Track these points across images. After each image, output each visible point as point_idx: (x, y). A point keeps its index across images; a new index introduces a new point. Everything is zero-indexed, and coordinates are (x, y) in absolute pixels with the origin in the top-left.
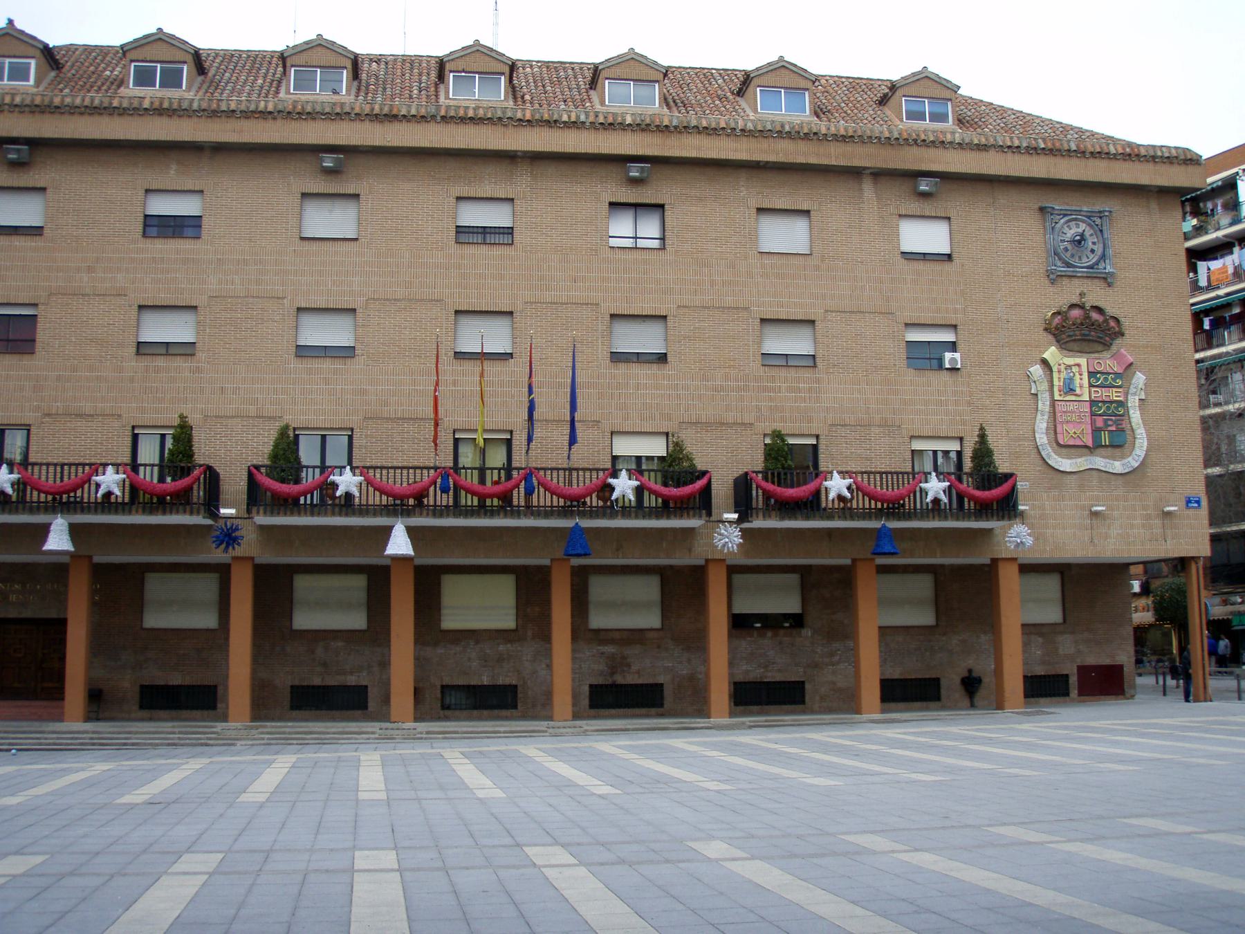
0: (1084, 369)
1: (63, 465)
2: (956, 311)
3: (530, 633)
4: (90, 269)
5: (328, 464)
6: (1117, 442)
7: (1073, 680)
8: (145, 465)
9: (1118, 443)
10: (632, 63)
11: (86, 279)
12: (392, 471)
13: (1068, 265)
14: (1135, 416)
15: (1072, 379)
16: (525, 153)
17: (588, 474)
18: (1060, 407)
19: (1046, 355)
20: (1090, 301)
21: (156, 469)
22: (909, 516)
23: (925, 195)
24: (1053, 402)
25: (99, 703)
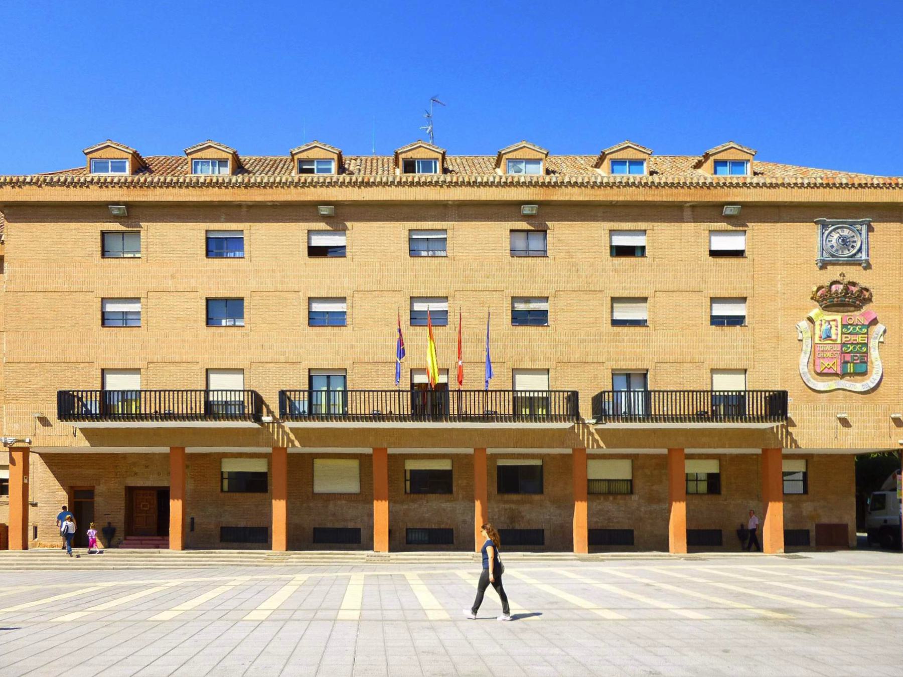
1: (160, 391)
2: (746, 288)
3: (460, 496)
4: (173, 277)
5: (517, 389)
6: (861, 369)
7: (813, 534)
8: (213, 391)
11: (170, 283)
13: (833, 256)
14: (874, 354)
17: (237, 393)
20: (849, 278)
21: (306, 394)
24: (814, 346)
25: (194, 540)
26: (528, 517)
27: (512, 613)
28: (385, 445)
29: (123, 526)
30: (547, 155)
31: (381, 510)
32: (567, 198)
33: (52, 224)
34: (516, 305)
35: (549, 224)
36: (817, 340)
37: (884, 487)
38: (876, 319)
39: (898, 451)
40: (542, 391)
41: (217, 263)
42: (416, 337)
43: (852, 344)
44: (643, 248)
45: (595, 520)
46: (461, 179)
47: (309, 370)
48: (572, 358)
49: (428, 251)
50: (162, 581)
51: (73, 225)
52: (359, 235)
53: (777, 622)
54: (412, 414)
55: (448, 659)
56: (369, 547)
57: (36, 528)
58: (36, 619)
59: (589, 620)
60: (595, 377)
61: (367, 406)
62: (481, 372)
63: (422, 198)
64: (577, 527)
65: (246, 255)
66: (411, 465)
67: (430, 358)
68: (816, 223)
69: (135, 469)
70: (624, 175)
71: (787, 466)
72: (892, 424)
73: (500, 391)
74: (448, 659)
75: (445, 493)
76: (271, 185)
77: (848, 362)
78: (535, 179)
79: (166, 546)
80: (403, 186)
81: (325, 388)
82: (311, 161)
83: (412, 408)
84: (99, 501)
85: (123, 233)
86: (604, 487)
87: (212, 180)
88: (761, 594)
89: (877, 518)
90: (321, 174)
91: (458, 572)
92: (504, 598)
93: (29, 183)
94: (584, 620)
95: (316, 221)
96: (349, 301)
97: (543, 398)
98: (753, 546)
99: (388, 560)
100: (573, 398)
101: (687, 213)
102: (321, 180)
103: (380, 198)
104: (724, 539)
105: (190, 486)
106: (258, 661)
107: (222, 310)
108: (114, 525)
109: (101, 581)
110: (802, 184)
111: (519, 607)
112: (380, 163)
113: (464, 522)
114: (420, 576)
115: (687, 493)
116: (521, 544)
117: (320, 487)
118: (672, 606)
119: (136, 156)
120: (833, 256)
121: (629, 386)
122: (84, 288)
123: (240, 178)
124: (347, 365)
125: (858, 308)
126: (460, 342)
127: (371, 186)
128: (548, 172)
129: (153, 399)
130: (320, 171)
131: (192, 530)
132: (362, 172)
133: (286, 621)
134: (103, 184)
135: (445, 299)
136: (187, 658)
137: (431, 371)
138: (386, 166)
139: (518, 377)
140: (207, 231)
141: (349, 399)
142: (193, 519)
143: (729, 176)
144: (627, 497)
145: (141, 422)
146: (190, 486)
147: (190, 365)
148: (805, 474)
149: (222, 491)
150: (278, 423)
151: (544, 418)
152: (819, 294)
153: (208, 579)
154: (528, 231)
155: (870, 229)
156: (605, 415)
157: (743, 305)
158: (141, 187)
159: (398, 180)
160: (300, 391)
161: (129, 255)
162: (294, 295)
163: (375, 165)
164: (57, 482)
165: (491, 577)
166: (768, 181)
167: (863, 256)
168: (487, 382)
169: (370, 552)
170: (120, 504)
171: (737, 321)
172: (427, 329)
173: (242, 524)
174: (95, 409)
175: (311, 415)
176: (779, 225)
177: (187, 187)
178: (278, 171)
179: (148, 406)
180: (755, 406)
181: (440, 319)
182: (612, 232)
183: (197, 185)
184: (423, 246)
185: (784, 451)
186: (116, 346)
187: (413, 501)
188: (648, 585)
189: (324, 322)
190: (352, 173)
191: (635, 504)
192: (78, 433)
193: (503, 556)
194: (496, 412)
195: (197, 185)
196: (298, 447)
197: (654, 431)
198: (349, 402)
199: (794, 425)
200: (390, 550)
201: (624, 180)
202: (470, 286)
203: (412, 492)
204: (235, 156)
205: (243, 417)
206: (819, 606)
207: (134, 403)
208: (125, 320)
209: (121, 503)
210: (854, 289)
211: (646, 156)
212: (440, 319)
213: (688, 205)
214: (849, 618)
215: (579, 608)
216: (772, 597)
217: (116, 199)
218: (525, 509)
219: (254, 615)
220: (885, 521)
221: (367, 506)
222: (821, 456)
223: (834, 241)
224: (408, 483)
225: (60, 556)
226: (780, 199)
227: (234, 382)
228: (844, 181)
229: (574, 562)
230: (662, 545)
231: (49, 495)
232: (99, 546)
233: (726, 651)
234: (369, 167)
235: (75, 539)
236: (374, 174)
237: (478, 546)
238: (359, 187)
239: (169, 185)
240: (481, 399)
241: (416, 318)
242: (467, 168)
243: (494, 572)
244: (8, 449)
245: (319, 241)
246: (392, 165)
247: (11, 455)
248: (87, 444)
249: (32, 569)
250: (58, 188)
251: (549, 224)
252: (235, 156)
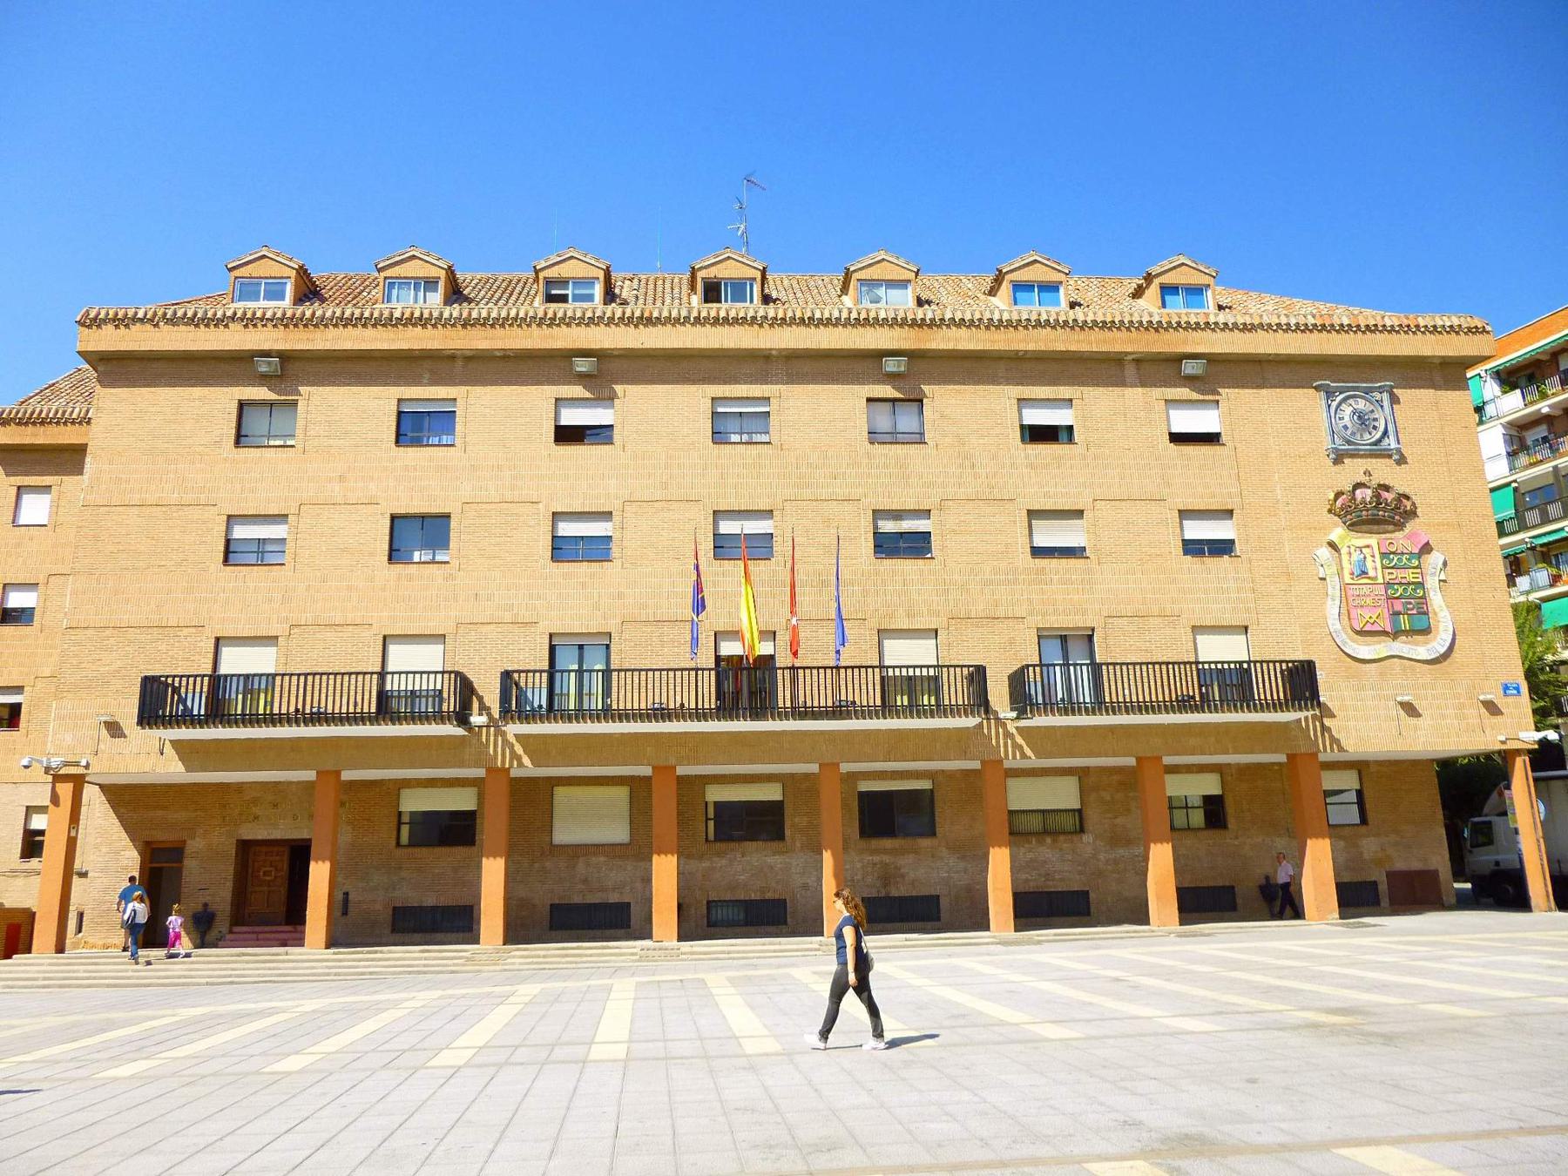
1: (306, 675)
4: (342, 478)
5: (390, 668)
7: (1383, 887)
12: (671, 674)
13: (1349, 442)
14: (1436, 600)
21: (545, 675)
24: (1344, 587)
26: (912, 875)
27: (888, 1036)
28: (672, 761)
29: (228, 908)
30: (917, 274)
31: (665, 872)
32: (951, 346)
33: (167, 390)
34: (880, 523)
35: (925, 388)
37: (1486, 810)
38: (1427, 543)
39: (1499, 752)
40: (928, 667)
41: (411, 454)
42: (724, 577)
44: (1070, 428)
45: (1024, 876)
46: (790, 314)
47: (551, 635)
48: (972, 612)
49: (741, 434)
50: (290, 1003)
51: (198, 391)
52: (637, 408)
53: (1334, 1030)
54: (718, 708)
55: (779, 1119)
56: (646, 934)
57: (81, 915)
58: (67, 1074)
59: (1020, 1042)
60: (1012, 642)
61: (643, 695)
62: (828, 636)
63: (732, 345)
64: (995, 889)
65: (458, 441)
66: (716, 794)
67: (746, 614)
68: (1316, 388)
69: (256, 810)
70: (1032, 308)
71: (1330, 781)
72: (1483, 710)
73: (859, 667)
74: (779, 1119)
75: (773, 839)
76: (502, 322)
77: (1399, 613)
78: (901, 315)
79: (300, 942)
80: (703, 325)
81: (576, 667)
82: (563, 282)
83: (718, 698)
84: (190, 865)
85: (271, 404)
86: (1035, 823)
87: (412, 316)
88: (1307, 986)
89: (1483, 859)
90: (578, 304)
91: (797, 973)
92: (873, 1011)
93: (141, 320)
94: (1013, 1042)
95: (569, 383)
96: (616, 518)
97: (929, 677)
98: (1288, 910)
99: (678, 955)
100: (978, 676)
101: (1130, 371)
102: (579, 315)
103: (668, 345)
104: (1239, 901)
105: (346, 837)
106: (449, 1138)
107: (414, 534)
108: (212, 908)
109: (185, 1006)
110: (1288, 324)
111: (900, 1026)
112: (668, 285)
113: (805, 887)
114: (730, 979)
115: (1172, 828)
116: (902, 920)
117: (565, 833)
118: (1159, 1013)
119: (302, 272)
120: (1349, 442)
121: (1066, 656)
122: (203, 499)
123: (455, 310)
124: (612, 626)
125: (1400, 526)
126: (793, 587)
127: (654, 325)
128: (920, 302)
129: (294, 689)
130: (577, 298)
131: (345, 913)
132: (641, 301)
133: (500, 1066)
134: (250, 321)
135: (768, 514)
136: (326, 1136)
137: (747, 636)
138: (676, 290)
139: (887, 643)
140: (399, 400)
141: (614, 684)
142: (346, 894)
143: (1184, 311)
144: (1075, 838)
145: (271, 729)
146: (346, 837)
147: (357, 630)
148: (1360, 793)
149: (398, 844)
150: (497, 727)
151: (932, 711)
152: (1339, 503)
153: (368, 998)
154: (894, 401)
155: (1394, 400)
156: (1032, 705)
157: (1228, 522)
158: (305, 326)
159: (695, 314)
160: (535, 672)
161: (278, 443)
162: (528, 508)
163: (660, 289)
164: (124, 835)
165: (852, 978)
166: (1240, 320)
167: (1391, 442)
168: (838, 652)
169: (647, 943)
170: (227, 870)
171: (1222, 548)
172: (741, 564)
173: (430, 901)
174: (198, 707)
175: (552, 711)
176: (1264, 392)
177: (374, 326)
178: (514, 298)
179: (285, 700)
180: (1268, 686)
181: (760, 547)
182: (1022, 402)
183: (390, 322)
184: (733, 425)
185: (1322, 757)
186: (245, 597)
187: (719, 854)
188: (1117, 980)
189: (577, 554)
190: (625, 303)
191: (1089, 850)
192: (168, 749)
193: (871, 943)
194: (854, 702)
195: (390, 322)
196: (527, 767)
197: (1112, 729)
198: (614, 689)
199: (1333, 716)
200: (680, 939)
201: (1034, 317)
202: (807, 493)
203: (718, 838)
204: (450, 271)
205: (439, 717)
206: (1403, 1001)
207: (262, 696)
208: (262, 553)
209: (228, 870)
210: (1389, 496)
211: (1062, 277)
212: (760, 547)
213: (1130, 357)
214: (1454, 1017)
215: (1002, 1023)
216: (1323, 989)
217: (266, 347)
218: (906, 862)
219: (447, 1058)
220: (1497, 863)
221: (642, 864)
222: (1380, 763)
223: (1347, 418)
224: (711, 824)
225: (119, 965)
226: (1261, 351)
227: (428, 657)
228: (1346, 321)
229: (992, 947)
230: (1139, 915)
231: (110, 855)
232: (185, 945)
233: (1253, 1081)
234: (651, 292)
235: (145, 935)
236: (659, 304)
237: (829, 927)
238: (636, 326)
239: (347, 322)
240: (829, 681)
241: (723, 547)
242: (799, 295)
243: (856, 970)
244: (50, 778)
245: (571, 417)
246: (685, 288)
247: (53, 788)
248: (180, 767)
249: (69, 986)
250: (183, 328)
251: (925, 388)
252: (450, 271)
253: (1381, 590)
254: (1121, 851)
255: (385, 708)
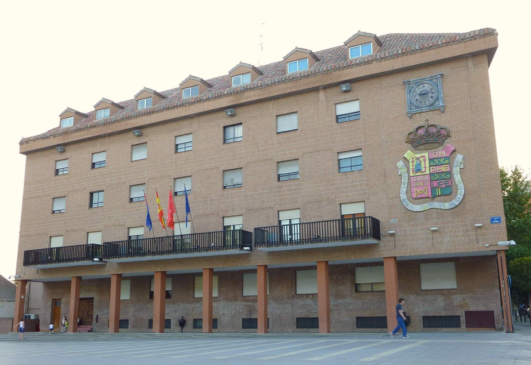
0: (427, 158)
2: (361, 142)
4: (78, 183)
6: (447, 192)
7: (463, 319)
9: (448, 191)
10: (240, 67)
14: (457, 178)
15: (420, 164)
16: (194, 114)
18: (413, 179)
19: (405, 155)
22: (144, 254)
23: (346, 92)
24: (409, 178)
36: (411, 174)
43: (438, 173)
142: (97, 316)
205: (365, 236)
222: (464, 258)
253: (427, 178)
254: (340, 301)
255: (343, 235)
